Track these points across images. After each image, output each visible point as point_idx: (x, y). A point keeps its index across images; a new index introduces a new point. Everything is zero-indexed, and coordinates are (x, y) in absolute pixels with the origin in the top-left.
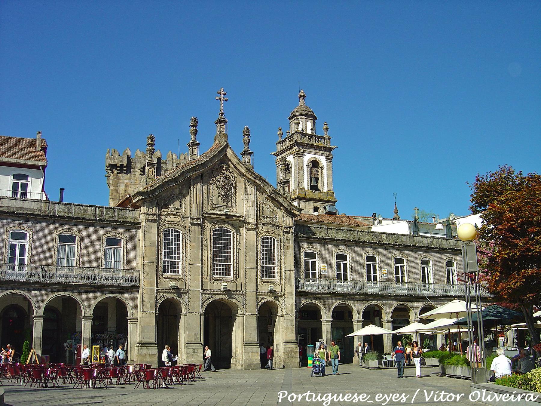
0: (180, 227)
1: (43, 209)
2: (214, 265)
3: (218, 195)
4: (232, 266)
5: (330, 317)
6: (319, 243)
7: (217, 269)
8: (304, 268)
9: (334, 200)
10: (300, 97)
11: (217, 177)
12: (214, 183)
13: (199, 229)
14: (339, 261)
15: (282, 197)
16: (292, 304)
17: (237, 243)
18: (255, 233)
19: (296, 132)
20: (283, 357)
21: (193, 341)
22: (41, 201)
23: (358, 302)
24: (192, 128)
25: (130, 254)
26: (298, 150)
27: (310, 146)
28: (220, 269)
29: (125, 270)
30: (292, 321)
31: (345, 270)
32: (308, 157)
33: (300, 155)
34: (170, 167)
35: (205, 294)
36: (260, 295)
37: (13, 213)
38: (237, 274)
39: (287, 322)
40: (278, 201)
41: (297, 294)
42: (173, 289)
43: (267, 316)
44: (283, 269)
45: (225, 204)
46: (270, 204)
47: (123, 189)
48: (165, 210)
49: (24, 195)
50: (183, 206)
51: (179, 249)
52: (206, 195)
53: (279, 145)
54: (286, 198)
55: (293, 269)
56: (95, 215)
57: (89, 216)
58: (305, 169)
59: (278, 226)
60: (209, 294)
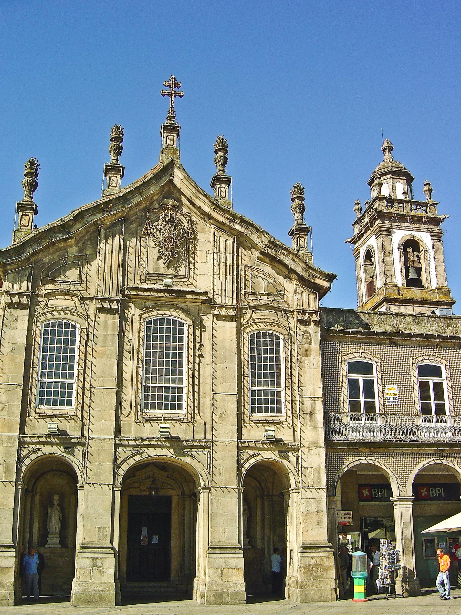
0: (76, 318)
2: (147, 388)
3: (157, 255)
4: (185, 391)
5: (408, 492)
6: (378, 344)
7: (153, 397)
8: (349, 392)
9: (446, 299)
11: (156, 224)
12: (148, 235)
13: (114, 319)
16: (319, 467)
17: (197, 346)
18: (234, 324)
27: (402, 218)
31: (439, 395)
32: (399, 236)
33: (387, 233)
36: (246, 448)
38: (195, 406)
39: (308, 504)
40: (281, 263)
41: (330, 445)
42: (56, 436)
44: (296, 393)
45: (171, 272)
46: (268, 269)
48: (47, 287)
50: (84, 277)
51: (72, 359)
52: (132, 257)
53: (357, 225)
55: (320, 393)
59: (285, 311)
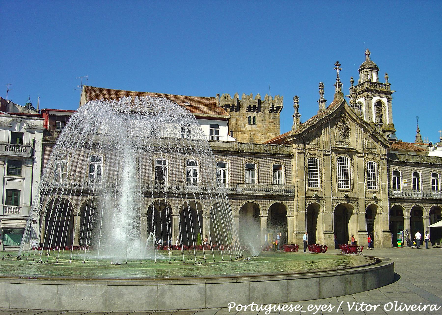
0: (317, 157)
1: (235, 147)
4: (349, 182)
8: (394, 183)
9: (392, 130)
10: (366, 54)
11: (339, 123)
12: (336, 127)
14: (415, 177)
15: (380, 135)
19: (366, 81)
20: (382, 240)
21: (328, 230)
22: (233, 142)
23: (427, 204)
24: (321, 90)
25: (288, 175)
26: (368, 95)
27: (377, 91)
28: (342, 183)
29: (286, 185)
30: (387, 217)
32: (375, 99)
33: (369, 98)
34: (267, 105)
35: (334, 200)
37: (219, 151)
39: (384, 218)
43: (371, 213)
45: (344, 141)
46: (372, 140)
47: (235, 122)
48: (308, 146)
49: (217, 138)
54: (382, 136)
56: (265, 150)
57: (262, 151)
58: (373, 107)
60: (336, 200)
